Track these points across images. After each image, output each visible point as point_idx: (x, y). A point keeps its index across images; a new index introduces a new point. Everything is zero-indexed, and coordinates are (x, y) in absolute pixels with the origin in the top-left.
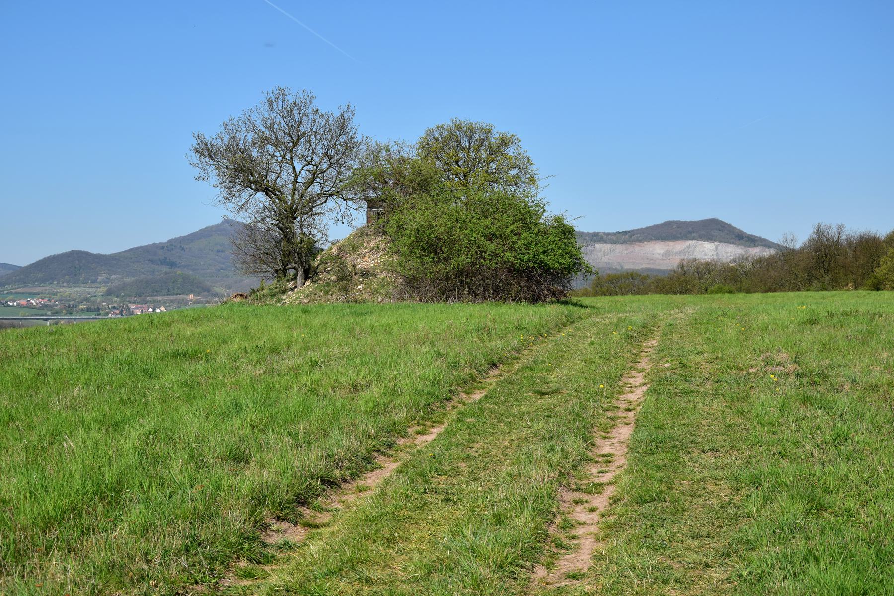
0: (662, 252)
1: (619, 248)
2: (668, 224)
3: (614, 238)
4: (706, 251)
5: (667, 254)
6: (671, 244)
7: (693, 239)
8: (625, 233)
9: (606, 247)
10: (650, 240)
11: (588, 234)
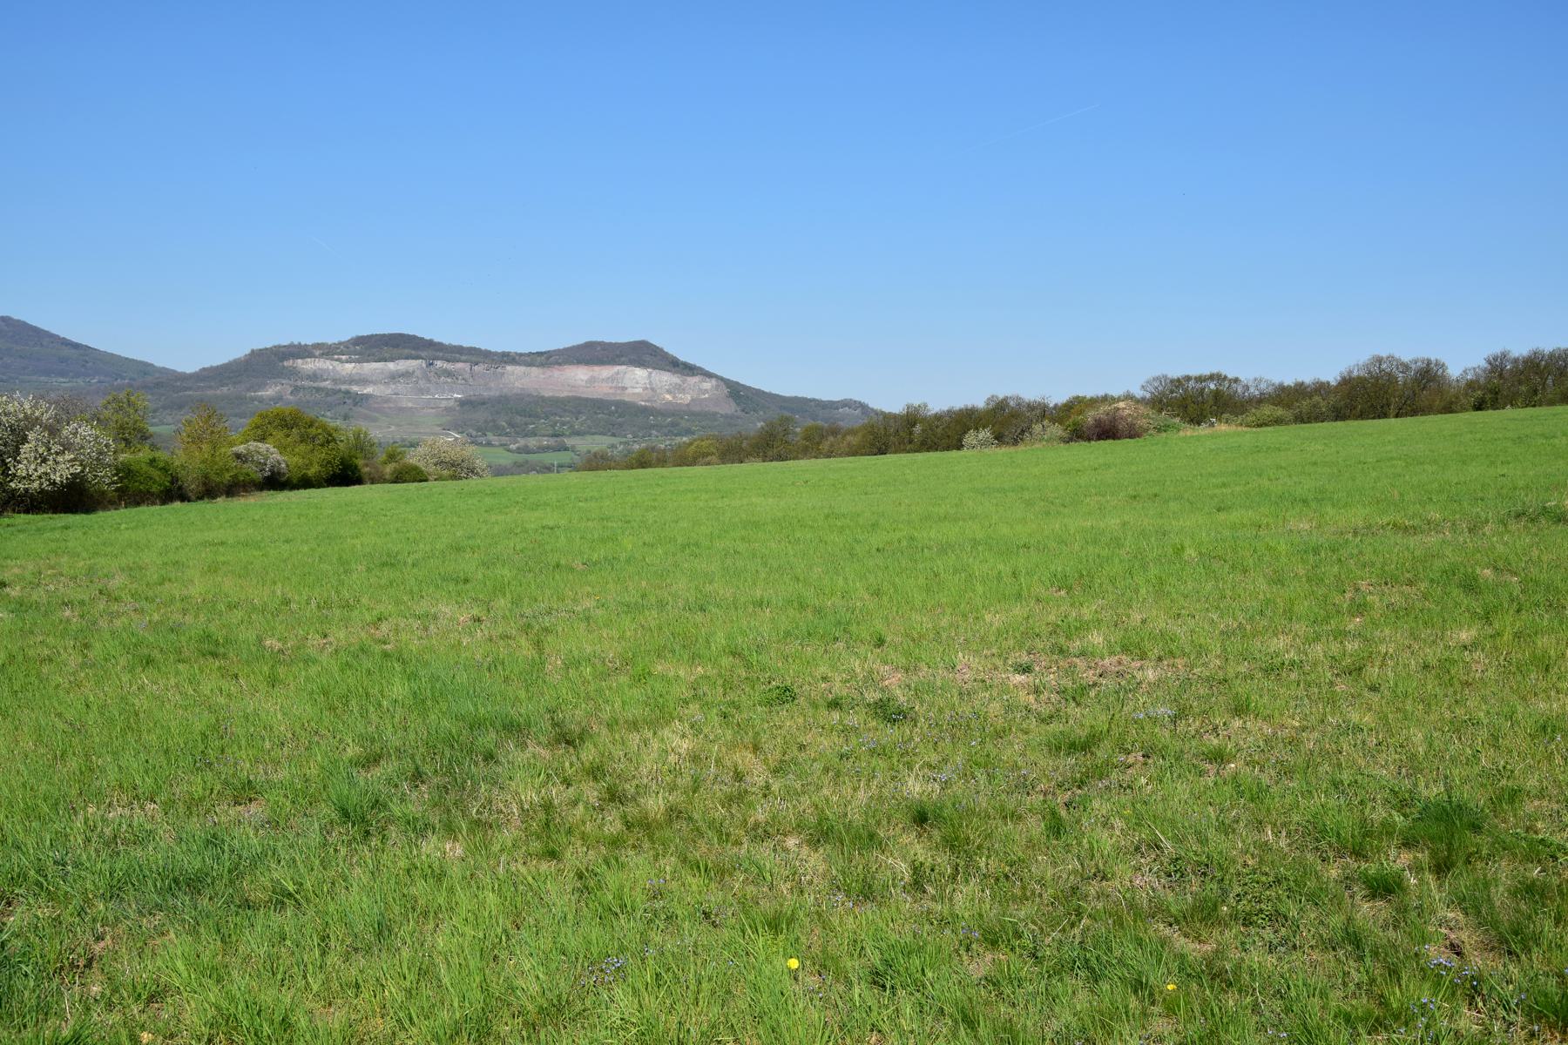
0: (585, 378)
1: (535, 371)
2: (590, 345)
3: (647, 358)
4: (637, 381)
5: (592, 380)
6: (596, 368)
7: (622, 364)
8: (540, 354)
9: (520, 369)
10: (572, 363)
11: (496, 354)
